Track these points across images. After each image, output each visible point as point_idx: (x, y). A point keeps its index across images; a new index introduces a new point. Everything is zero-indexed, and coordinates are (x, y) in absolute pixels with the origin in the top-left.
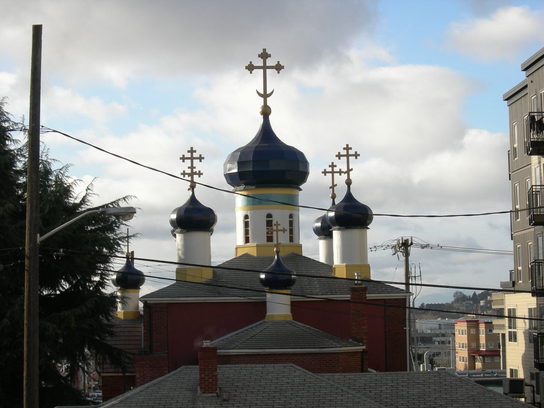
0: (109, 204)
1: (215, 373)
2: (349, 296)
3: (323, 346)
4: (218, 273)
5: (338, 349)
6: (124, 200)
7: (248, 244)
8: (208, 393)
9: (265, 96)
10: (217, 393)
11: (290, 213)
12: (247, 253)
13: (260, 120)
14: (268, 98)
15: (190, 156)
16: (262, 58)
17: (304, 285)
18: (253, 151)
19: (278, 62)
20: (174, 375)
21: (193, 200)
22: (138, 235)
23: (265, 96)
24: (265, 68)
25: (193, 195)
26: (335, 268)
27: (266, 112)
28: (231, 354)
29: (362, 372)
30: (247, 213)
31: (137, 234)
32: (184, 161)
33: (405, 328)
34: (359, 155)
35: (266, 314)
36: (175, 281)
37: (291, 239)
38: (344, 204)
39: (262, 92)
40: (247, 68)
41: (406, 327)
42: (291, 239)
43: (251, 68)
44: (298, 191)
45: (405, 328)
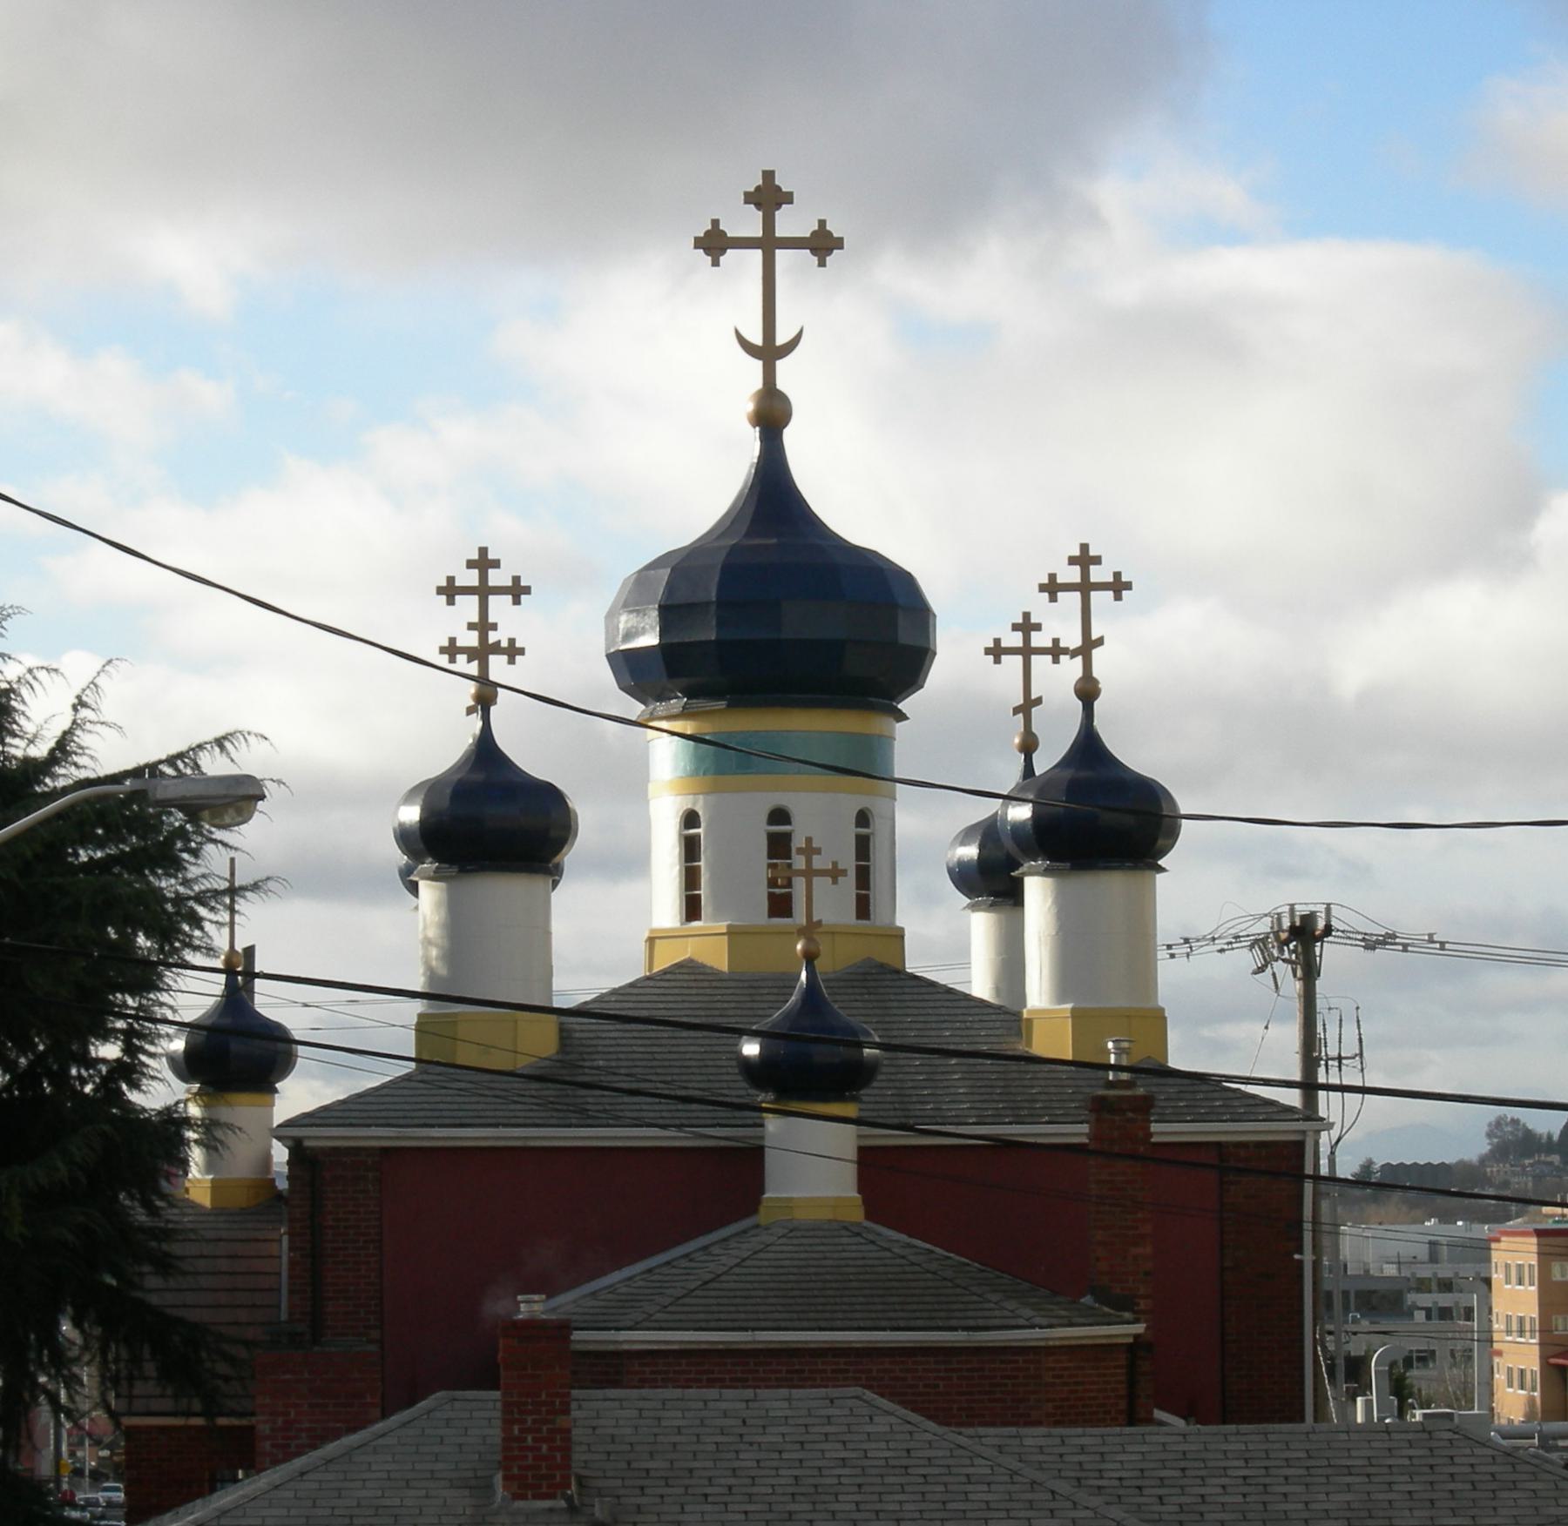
0: (161, 762)
1: (561, 1421)
2: (1085, 1128)
3: (981, 1322)
4: (577, 1035)
6: (217, 749)
7: (695, 924)
8: (536, 1497)
9: (769, 352)
10: (569, 1500)
11: (858, 808)
12: (690, 960)
13: (750, 445)
14: (779, 363)
15: (1078, 579)
16: (758, 206)
17: (910, 1084)
18: (719, 566)
19: (822, 223)
20: (404, 1425)
21: (486, 750)
22: (271, 884)
23: (769, 352)
24: (769, 244)
26: (1029, 1021)
28: (626, 1347)
30: (694, 804)
31: (268, 879)
32: (451, 602)
33: (1297, 1257)
34: (440, 591)
35: (763, 1193)
36: (413, 1065)
37: (863, 908)
38: (1068, 774)
39: (757, 338)
40: (699, 243)
41: (1301, 1252)
42: (863, 908)
43: (714, 243)
44: (891, 720)
45: (1297, 1257)
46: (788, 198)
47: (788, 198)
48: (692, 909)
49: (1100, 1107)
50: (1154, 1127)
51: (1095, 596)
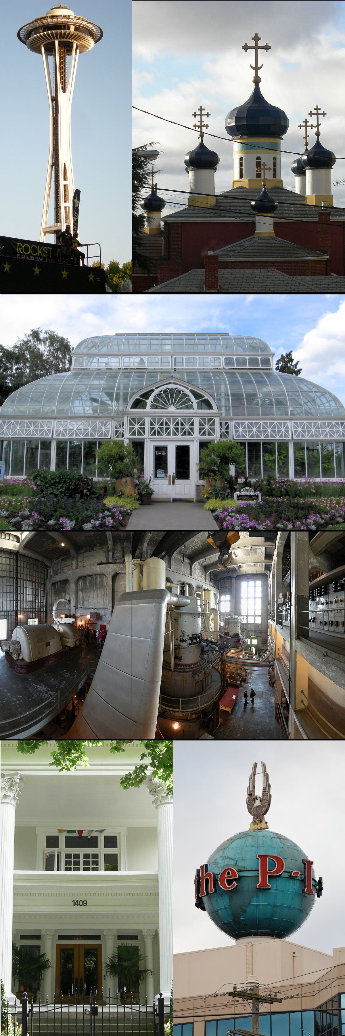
5: (308, 258)
9: (256, 69)
16: (254, 40)
20: (186, 276)
21: (202, 145)
23: (256, 69)
24: (256, 48)
25: (202, 142)
27: (257, 81)
29: (326, 275)
32: (195, 117)
37: (275, 176)
38: (314, 150)
39: (254, 66)
40: (243, 48)
42: (275, 176)
43: (246, 48)
46: (260, 39)
47: (260, 39)
48: (242, 176)
49: (320, 214)
50: (331, 218)
51: (203, 116)
